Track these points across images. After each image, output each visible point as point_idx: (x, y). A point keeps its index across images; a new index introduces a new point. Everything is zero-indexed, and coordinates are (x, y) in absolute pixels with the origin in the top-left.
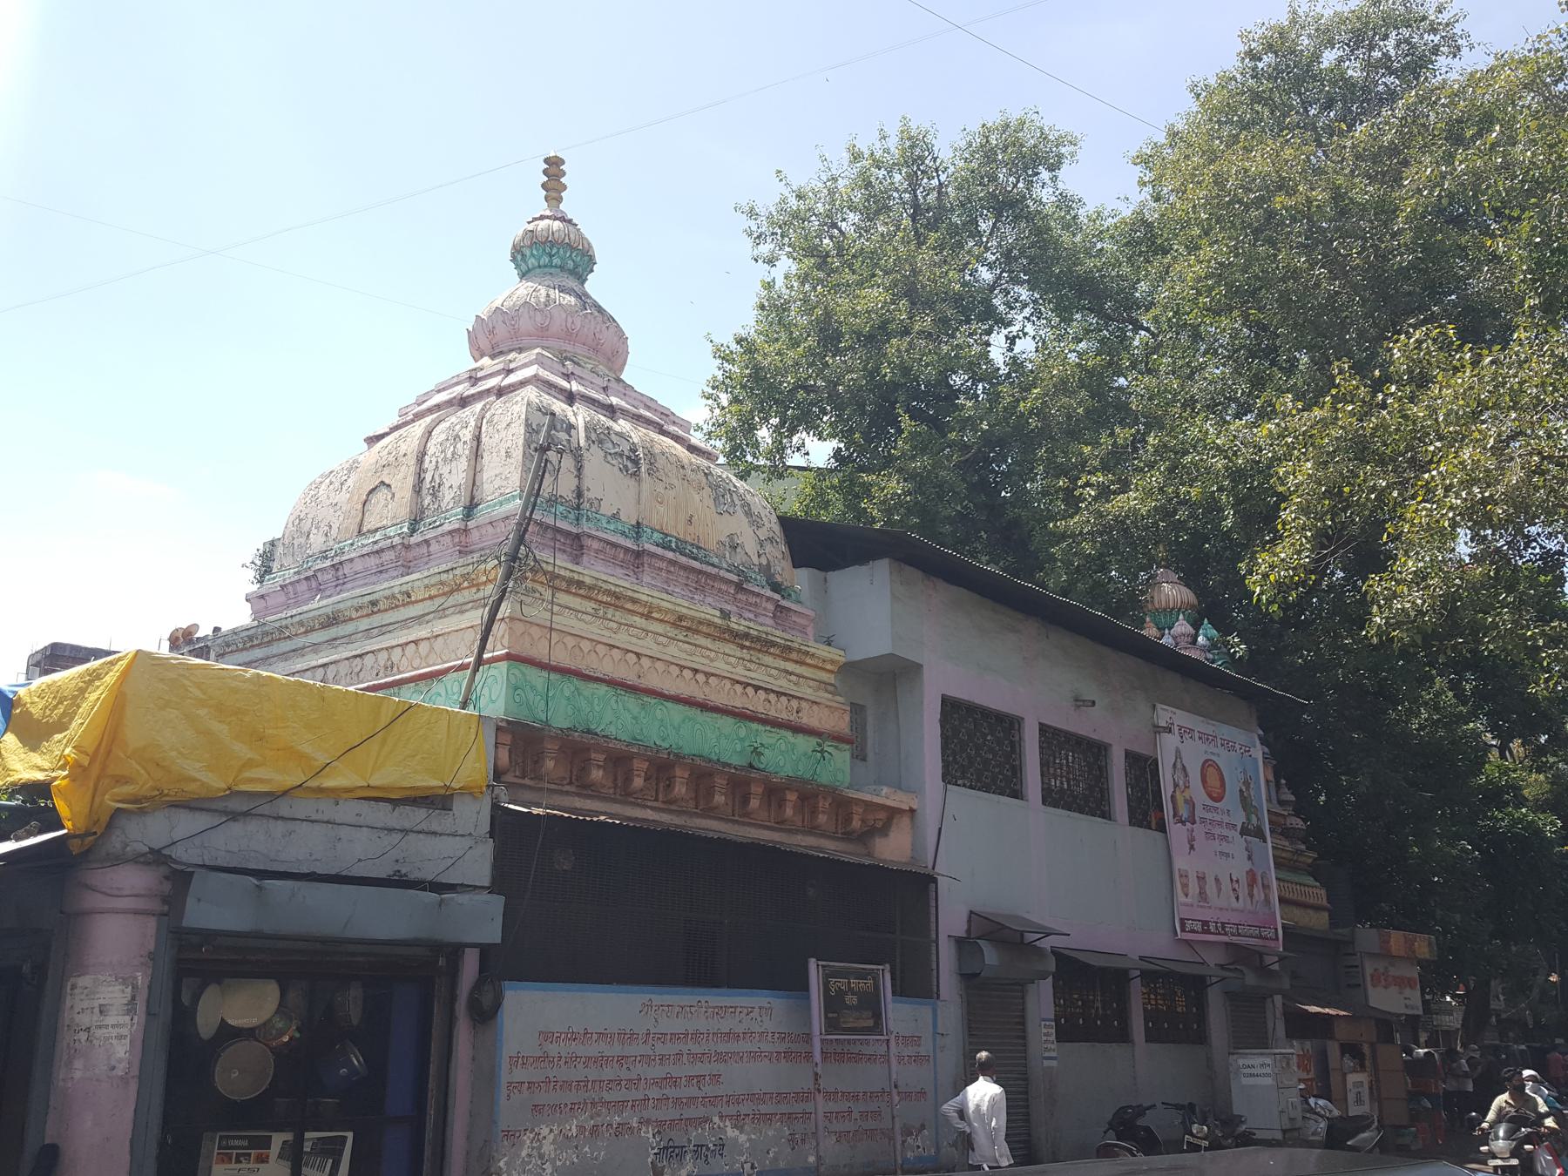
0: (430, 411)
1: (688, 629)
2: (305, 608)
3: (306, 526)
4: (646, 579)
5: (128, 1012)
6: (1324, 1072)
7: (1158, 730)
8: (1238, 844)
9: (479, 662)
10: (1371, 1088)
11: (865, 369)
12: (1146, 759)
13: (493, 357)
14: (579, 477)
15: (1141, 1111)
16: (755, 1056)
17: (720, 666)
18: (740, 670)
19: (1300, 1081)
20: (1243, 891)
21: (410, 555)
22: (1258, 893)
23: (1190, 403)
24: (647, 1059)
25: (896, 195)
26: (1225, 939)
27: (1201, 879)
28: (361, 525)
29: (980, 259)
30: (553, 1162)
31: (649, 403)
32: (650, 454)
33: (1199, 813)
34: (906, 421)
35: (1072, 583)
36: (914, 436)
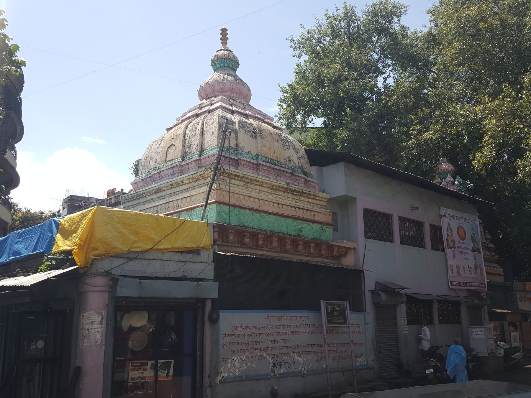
0: (187, 119)
1: (275, 189)
2: (150, 187)
3: (149, 159)
4: (261, 173)
5: (101, 324)
6: (503, 332)
7: (441, 216)
8: (471, 255)
9: (207, 204)
10: (520, 337)
11: (333, 93)
12: (437, 226)
13: (206, 99)
14: (236, 139)
15: (438, 348)
16: (303, 332)
17: (287, 202)
18: (294, 203)
19: (494, 335)
20: (473, 271)
21: (183, 168)
22: (478, 271)
23: (450, 99)
24: (268, 334)
25: (342, 30)
26: (467, 288)
27: (458, 267)
28: (166, 159)
29: (374, 51)
30: (239, 369)
31: (259, 112)
32: (260, 130)
33: (457, 244)
34: (348, 110)
35: (409, 164)
36: (351, 115)
